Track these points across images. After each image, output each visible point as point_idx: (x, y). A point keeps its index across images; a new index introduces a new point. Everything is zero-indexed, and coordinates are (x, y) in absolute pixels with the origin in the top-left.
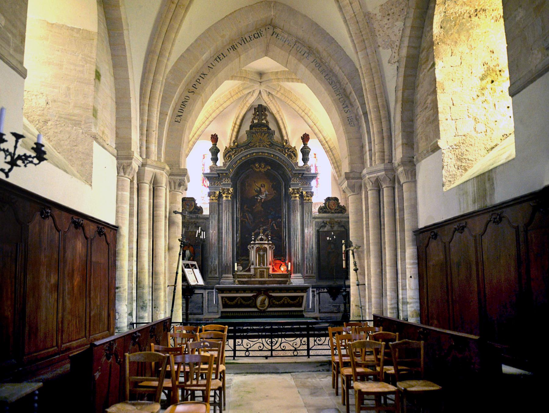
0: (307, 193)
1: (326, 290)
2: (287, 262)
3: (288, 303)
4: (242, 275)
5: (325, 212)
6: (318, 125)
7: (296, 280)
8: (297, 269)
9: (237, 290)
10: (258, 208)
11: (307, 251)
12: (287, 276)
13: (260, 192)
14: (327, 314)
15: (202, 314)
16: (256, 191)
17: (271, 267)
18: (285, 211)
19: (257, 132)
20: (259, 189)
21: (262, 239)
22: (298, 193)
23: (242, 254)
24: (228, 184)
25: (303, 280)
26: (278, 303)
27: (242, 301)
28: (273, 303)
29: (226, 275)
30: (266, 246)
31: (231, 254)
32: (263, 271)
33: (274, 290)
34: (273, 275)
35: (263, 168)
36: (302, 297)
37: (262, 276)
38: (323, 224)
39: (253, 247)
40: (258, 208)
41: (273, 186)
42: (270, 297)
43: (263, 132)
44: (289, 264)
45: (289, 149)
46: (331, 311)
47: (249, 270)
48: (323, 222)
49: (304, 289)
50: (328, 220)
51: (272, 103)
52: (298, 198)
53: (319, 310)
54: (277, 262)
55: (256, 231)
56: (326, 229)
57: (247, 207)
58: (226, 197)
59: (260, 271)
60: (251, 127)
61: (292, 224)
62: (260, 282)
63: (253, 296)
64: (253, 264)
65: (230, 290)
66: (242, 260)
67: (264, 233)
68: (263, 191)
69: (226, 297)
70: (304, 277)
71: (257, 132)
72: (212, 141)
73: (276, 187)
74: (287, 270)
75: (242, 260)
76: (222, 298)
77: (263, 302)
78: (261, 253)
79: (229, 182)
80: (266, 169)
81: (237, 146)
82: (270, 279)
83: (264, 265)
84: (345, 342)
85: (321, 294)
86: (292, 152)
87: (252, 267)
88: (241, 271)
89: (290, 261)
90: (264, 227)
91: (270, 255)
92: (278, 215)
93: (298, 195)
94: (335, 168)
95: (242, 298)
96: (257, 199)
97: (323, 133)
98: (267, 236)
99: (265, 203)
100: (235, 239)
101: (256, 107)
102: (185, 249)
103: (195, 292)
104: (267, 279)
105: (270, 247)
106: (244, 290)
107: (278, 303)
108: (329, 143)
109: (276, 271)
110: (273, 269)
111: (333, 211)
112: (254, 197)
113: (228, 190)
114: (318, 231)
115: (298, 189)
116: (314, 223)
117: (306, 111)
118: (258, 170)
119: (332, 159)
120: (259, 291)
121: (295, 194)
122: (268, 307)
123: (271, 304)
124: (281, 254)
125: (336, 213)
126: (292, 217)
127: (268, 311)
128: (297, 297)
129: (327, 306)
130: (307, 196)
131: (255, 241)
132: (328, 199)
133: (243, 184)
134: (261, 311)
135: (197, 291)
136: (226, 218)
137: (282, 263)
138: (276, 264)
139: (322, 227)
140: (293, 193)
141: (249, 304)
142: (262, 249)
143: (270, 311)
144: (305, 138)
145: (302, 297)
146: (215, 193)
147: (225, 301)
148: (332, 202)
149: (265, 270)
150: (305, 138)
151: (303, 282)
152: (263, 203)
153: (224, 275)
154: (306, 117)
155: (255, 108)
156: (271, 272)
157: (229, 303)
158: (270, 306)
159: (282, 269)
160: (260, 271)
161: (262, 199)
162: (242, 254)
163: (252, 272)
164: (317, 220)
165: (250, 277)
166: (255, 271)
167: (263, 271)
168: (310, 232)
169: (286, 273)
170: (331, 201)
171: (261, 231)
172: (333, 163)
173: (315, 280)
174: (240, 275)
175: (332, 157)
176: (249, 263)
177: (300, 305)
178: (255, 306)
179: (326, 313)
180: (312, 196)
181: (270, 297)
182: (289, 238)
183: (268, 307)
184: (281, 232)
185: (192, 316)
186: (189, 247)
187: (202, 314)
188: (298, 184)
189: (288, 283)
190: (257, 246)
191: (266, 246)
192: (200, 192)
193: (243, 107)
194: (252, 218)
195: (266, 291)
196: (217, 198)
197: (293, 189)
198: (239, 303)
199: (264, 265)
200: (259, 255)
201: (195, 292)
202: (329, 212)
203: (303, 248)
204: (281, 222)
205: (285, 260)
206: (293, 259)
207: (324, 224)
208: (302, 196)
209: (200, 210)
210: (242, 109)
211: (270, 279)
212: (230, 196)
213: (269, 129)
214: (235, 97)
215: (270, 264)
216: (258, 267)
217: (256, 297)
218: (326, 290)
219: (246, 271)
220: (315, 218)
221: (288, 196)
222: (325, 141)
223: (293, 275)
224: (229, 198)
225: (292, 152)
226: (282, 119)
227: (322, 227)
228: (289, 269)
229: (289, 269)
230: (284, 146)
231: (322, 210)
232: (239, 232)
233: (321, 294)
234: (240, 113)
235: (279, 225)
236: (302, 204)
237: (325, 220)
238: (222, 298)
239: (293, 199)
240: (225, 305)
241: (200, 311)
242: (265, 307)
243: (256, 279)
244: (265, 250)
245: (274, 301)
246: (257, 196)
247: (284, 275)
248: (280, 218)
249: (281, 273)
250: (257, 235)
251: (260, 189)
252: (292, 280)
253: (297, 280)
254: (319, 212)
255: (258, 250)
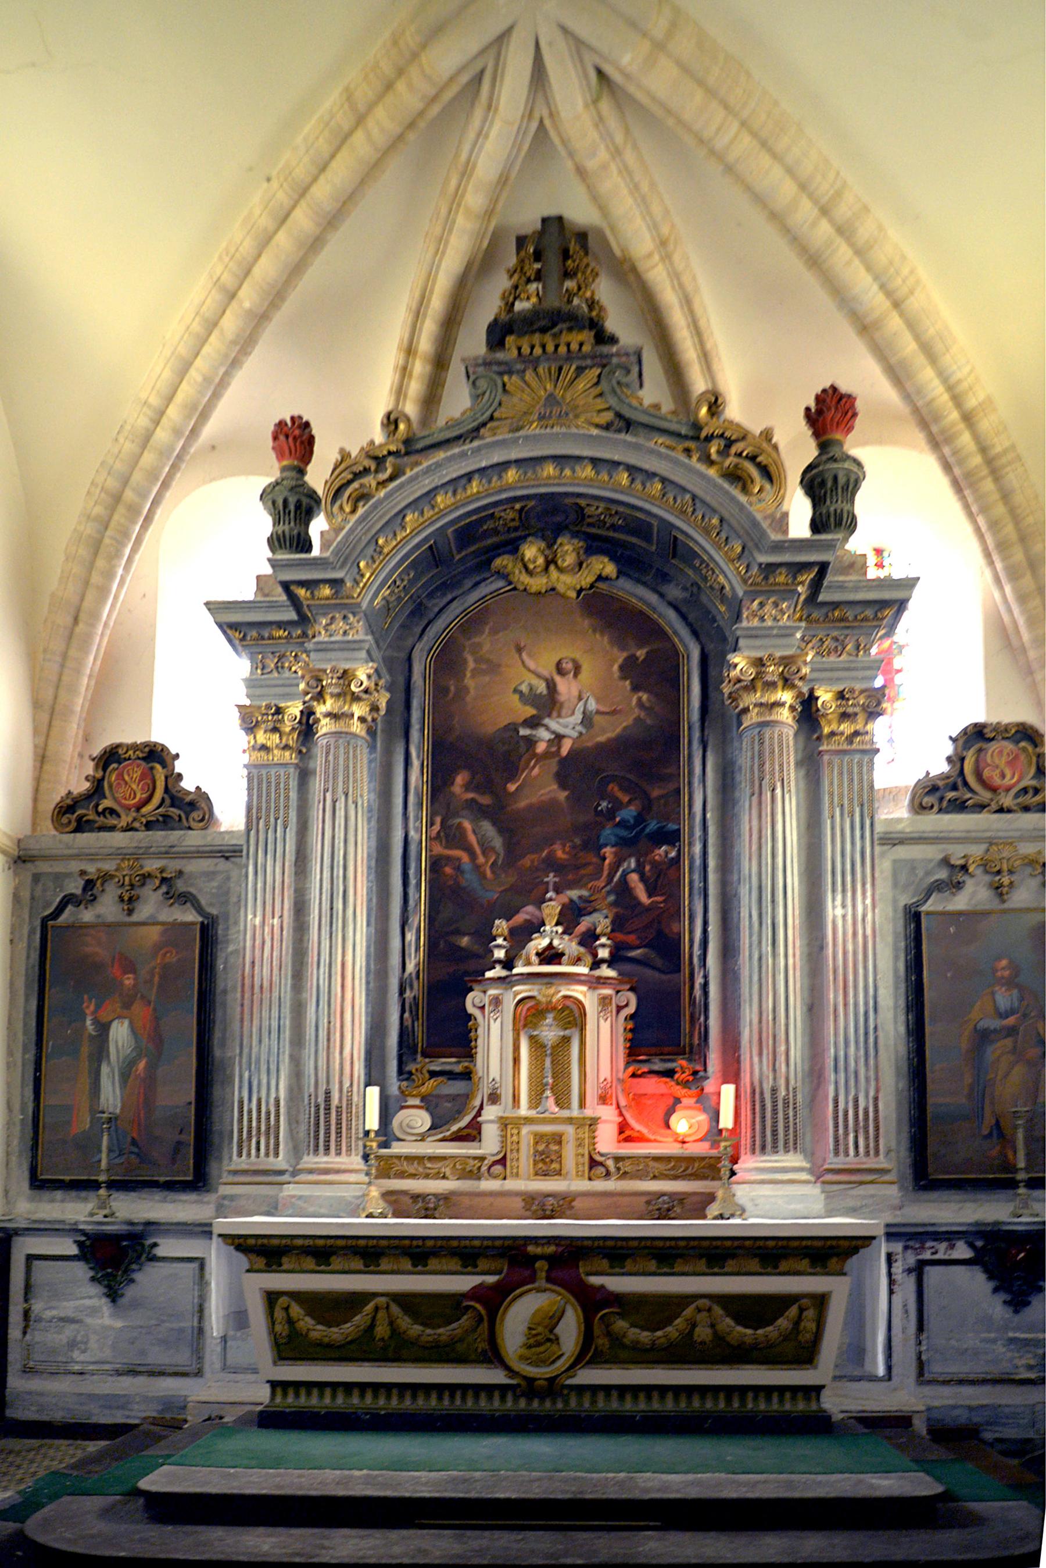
0: (841, 696)
1: (962, 1251)
2: (709, 1086)
3: (719, 1338)
4: (420, 1159)
5: (959, 806)
6: (915, 303)
7: (766, 1190)
8: (772, 1124)
9: (370, 1252)
10: (538, 787)
11: (840, 1030)
12: (712, 1167)
13: (548, 703)
14: (967, 1391)
15: (199, 1373)
16: (530, 698)
17: (608, 1115)
18: (701, 795)
19: (535, 363)
20: (542, 688)
21: (550, 956)
22: (787, 683)
23: (431, 1033)
24: (349, 647)
25: (815, 1191)
26: (645, 1337)
27: (405, 1322)
28: (616, 1340)
29: (322, 1160)
30: (578, 991)
31: (871, 1189)
32: (558, 1139)
33: (618, 1252)
34: (618, 1159)
35: (568, 571)
36: (821, 1301)
37: (547, 1161)
38: (943, 874)
39: (497, 1001)
40: (538, 787)
41: (628, 668)
42: (593, 1303)
43: (570, 356)
44: (728, 1092)
45: (730, 443)
46: (995, 1371)
47: (472, 1133)
48: (946, 862)
49: (828, 1252)
50: (977, 851)
51: (626, 171)
52: (785, 715)
53: (921, 1366)
54: (652, 1085)
55: (520, 918)
56: (960, 902)
57: (467, 787)
58: (332, 715)
59: (539, 1138)
60: (498, 334)
61: (747, 866)
62: (539, 1206)
63: (476, 1293)
64: (494, 1098)
65: (322, 1251)
66: (433, 1074)
67: (569, 918)
68: (562, 685)
69: (296, 1296)
70: (820, 1174)
71: (535, 363)
72: (280, 455)
73: (654, 672)
74: (715, 1133)
75: (433, 1074)
76: (271, 1298)
77: (542, 1335)
78: (549, 1032)
79: (359, 632)
80: (586, 579)
81: (407, 442)
82: (601, 1185)
83: (562, 1102)
84: (331, 684)
85: (933, 1274)
86: (752, 458)
87: (491, 1113)
88: (422, 1137)
89: (732, 1073)
90: (574, 894)
91: (603, 1040)
92: (656, 831)
93: (787, 697)
94: (1014, 574)
95: (407, 1301)
96: (531, 742)
97: (946, 360)
98: (589, 939)
99: (578, 768)
100: (395, 960)
101: (528, 230)
102: (104, 1017)
103: (160, 1252)
104: (582, 1185)
105: (604, 1001)
106: (419, 1253)
107: (645, 1337)
108: (986, 424)
109: (641, 1139)
110: (623, 1127)
111: (1007, 801)
112: (513, 728)
113: (346, 676)
114: (914, 917)
115: (786, 661)
116: (885, 866)
117: (843, 211)
118: (537, 583)
119: (994, 525)
120: (516, 1259)
121: (771, 686)
122: (581, 1360)
123: (602, 1342)
124: (666, 1034)
125: (1026, 809)
126: (746, 823)
127: (581, 1389)
128: (781, 1302)
129: (971, 1341)
130: (844, 716)
131: (508, 964)
132: (976, 735)
133: (447, 661)
134: (529, 1388)
135: (167, 1247)
136: (346, 840)
137: (679, 1091)
138: (638, 1100)
139: (937, 887)
140: (751, 687)
141: (453, 1342)
142: (550, 1008)
143: (594, 1389)
144: (830, 414)
145: (821, 1301)
146: (279, 711)
147: (290, 1322)
148: (998, 755)
149: (570, 1130)
150: (830, 414)
151: (819, 1206)
152: (564, 762)
153: (310, 1160)
154: (842, 254)
155: (521, 242)
156: (607, 1141)
157: (318, 1331)
158: (588, 1354)
159: (682, 1124)
160: (539, 1138)
161: (559, 738)
162: (431, 1033)
163: (490, 1143)
164: (902, 852)
165: (471, 1170)
166: (504, 1139)
167: (558, 1139)
168: (863, 920)
169: (702, 1149)
170: (993, 746)
171: (552, 909)
172: (1002, 546)
173: (893, 1192)
174: (410, 1159)
175: (1000, 510)
176: (467, 1097)
177: (806, 1354)
178: (493, 1356)
179: (961, 1382)
180: (873, 714)
181: (593, 1303)
182: (729, 951)
183: (581, 1360)
184: (677, 914)
185: (141, 1380)
186: (127, 1005)
187: (199, 1373)
188: (786, 633)
189: (713, 1209)
190: (523, 990)
191: (578, 991)
192: (199, 709)
193: (448, 224)
194: (498, 843)
195: (568, 1259)
196: (292, 740)
197: (759, 663)
198: (382, 1330)
199: (562, 1102)
200: (536, 1043)
201: (160, 1252)
202: (981, 807)
203: (814, 1008)
204: (677, 861)
205: (697, 1077)
206: (752, 1064)
207: (956, 875)
208: (808, 712)
209: (192, 808)
210: (442, 241)
211: (601, 1185)
212: (359, 710)
213: (603, 338)
214: (383, 122)
215: (603, 1099)
216: (524, 1111)
217: (494, 1300)
218: (962, 1251)
219: (459, 1137)
220: (892, 840)
221: (719, 717)
222: (955, 415)
223: (747, 1164)
224: (356, 727)
225: (752, 458)
226: (687, 302)
227: (937, 887)
228: (727, 1121)
229: (727, 1121)
230: (697, 427)
231: (938, 795)
232: (419, 919)
233: (933, 1274)
234: (430, 278)
235: (665, 880)
236: (811, 763)
237: (957, 853)
238: (271, 1298)
239: (752, 718)
240: (289, 1346)
241: (182, 1358)
242: (561, 1365)
243: (511, 1185)
244: (572, 1016)
245: (621, 1324)
246: (533, 723)
247: (690, 1160)
248: (672, 838)
249: (668, 1148)
250: (521, 935)
251: (552, 686)
252: (742, 1193)
253: (774, 1196)
254: (919, 807)
255: (530, 1015)
